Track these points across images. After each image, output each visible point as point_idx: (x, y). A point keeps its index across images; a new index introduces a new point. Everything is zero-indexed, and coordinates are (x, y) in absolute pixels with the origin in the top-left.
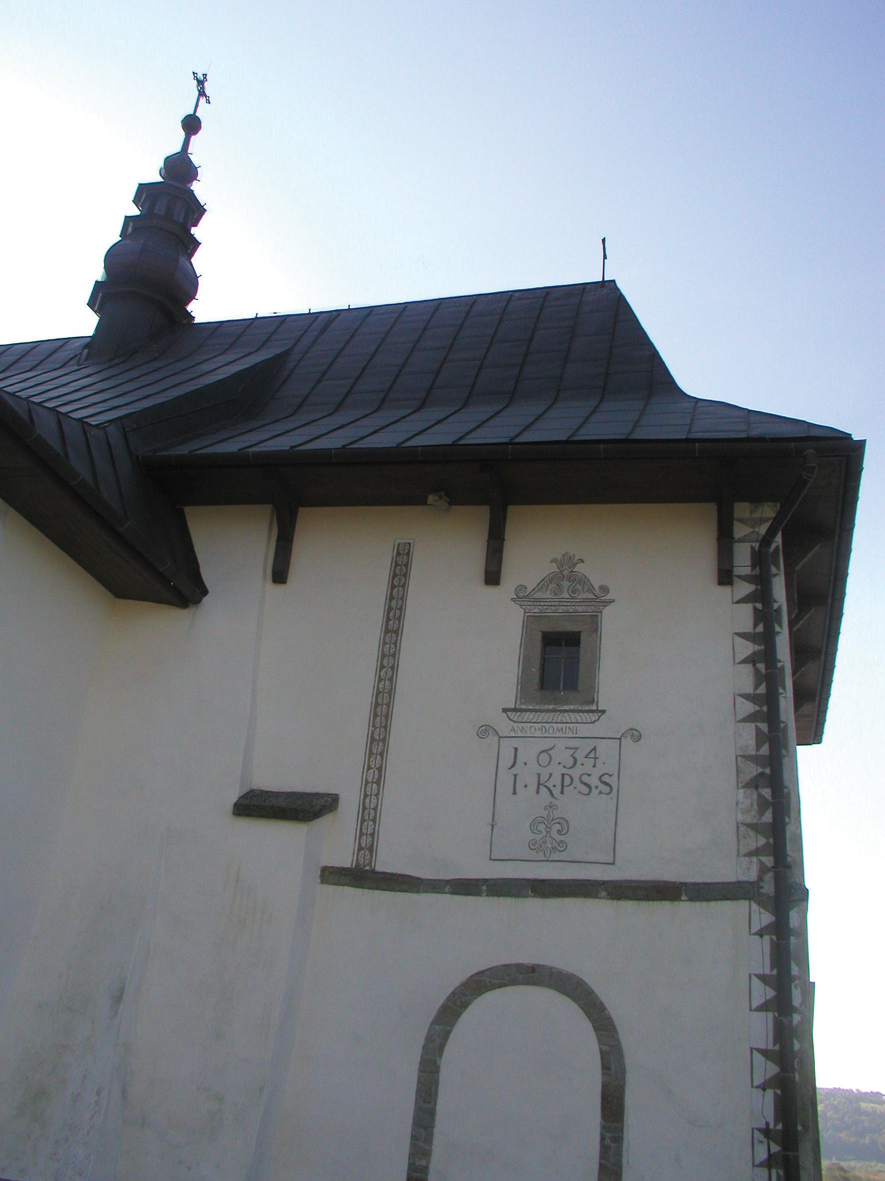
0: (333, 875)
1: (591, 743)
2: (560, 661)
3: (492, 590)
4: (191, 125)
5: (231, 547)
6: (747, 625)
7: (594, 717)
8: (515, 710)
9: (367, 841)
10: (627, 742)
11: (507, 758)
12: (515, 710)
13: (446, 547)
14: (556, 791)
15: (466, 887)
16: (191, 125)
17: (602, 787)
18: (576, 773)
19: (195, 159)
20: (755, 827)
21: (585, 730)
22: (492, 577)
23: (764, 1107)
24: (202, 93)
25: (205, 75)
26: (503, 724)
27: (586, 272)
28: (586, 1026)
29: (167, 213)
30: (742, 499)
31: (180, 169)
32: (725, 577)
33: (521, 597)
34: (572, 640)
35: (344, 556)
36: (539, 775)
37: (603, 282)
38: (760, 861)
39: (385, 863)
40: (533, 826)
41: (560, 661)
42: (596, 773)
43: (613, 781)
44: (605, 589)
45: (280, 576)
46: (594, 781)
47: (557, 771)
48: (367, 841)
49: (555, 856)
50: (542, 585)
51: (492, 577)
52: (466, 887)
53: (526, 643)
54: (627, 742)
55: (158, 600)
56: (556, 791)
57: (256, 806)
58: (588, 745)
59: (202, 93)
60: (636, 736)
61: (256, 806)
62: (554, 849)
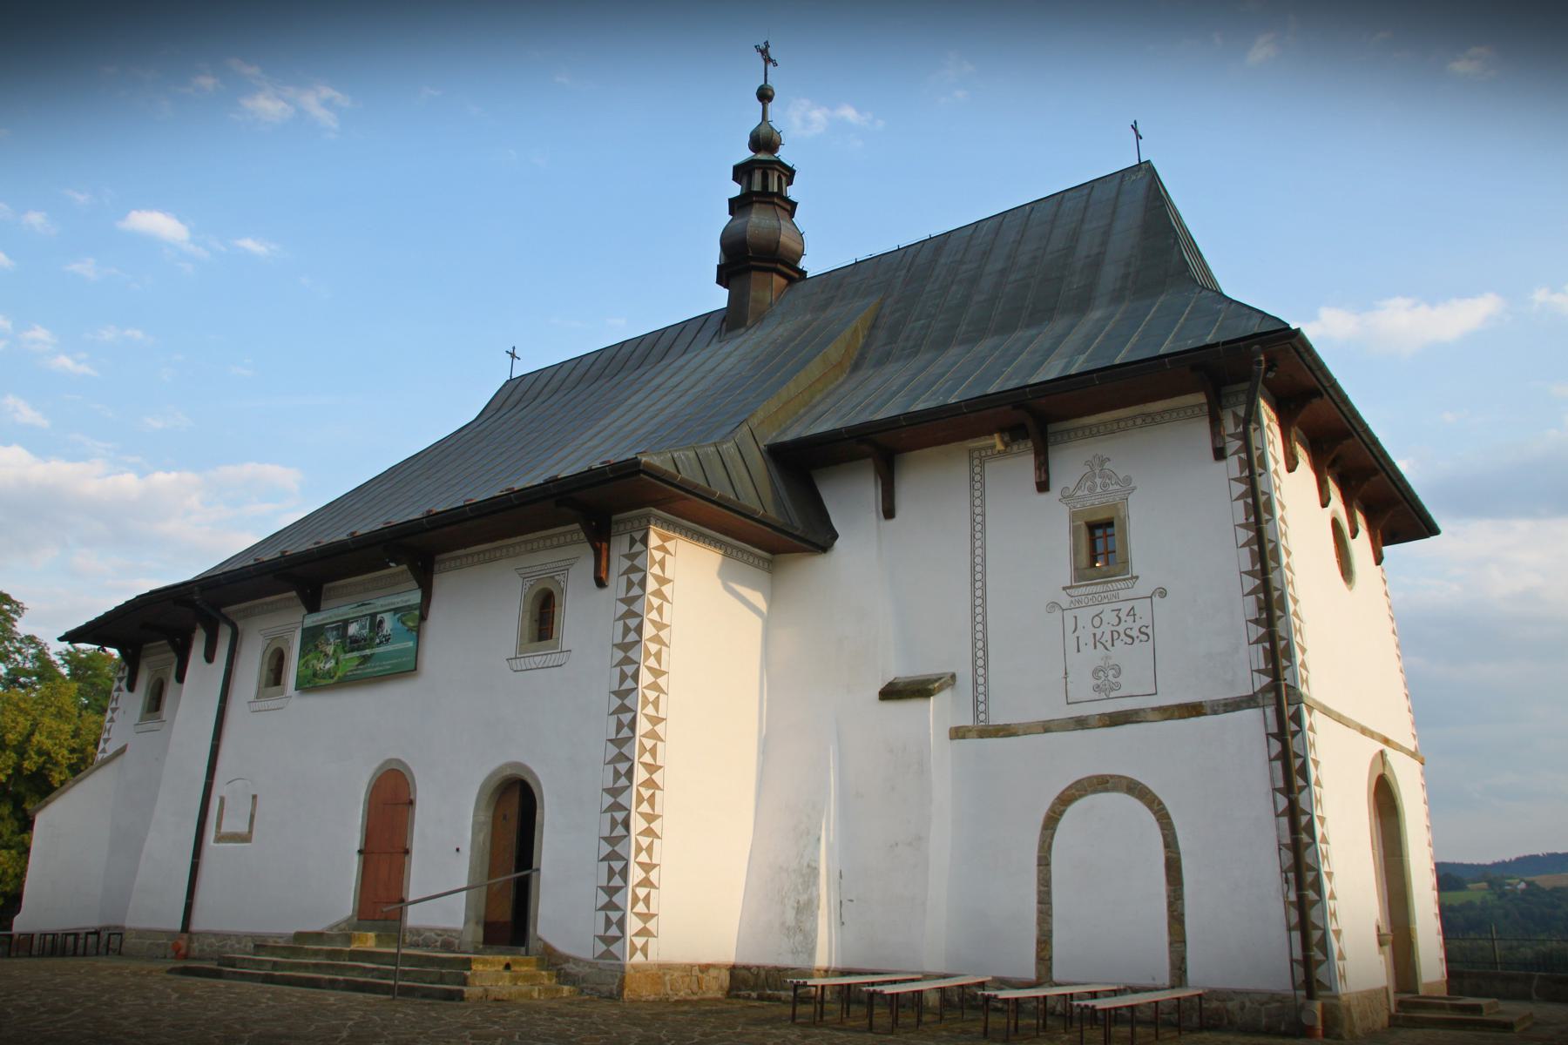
0: (958, 733)
1: (1130, 604)
2: (1100, 542)
3: (1044, 496)
4: (765, 95)
7: (1129, 583)
8: (1071, 587)
9: (979, 701)
10: (1156, 599)
11: (1070, 625)
12: (1071, 587)
14: (1109, 645)
15: (1047, 727)
16: (765, 95)
17: (1144, 637)
18: (1121, 629)
19: (776, 126)
21: (1123, 594)
22: (1043, 486)
24: (768, 60)
25: (766, 43)
26: (1065, 601)
28: (1072, 811)
30: (1208, 397)
31: (764, 141)
32: (1219, 454)
33: (1065, 497)
34: (1109, 524)
35: (935, 493)
36: (1387, 508)
39: (998, 718)
40: (1095, 672)
41: (1100, 542)
42: (1136, 627)
43: (1149, 631)
44: (1128, 480)
45: (889, 512)
46: (1134, 633)
47: (1107, 629)
48: (979, 701)
49: (1113, 694)
50: (1078, 487)
51: (1043, 486)
52: (1047, 727)
53: (1075, 532)
54: (1156, 599)
55: (804, 551)
56: (1109, 645)
58: (1125, 607)
59: (768, 60)
60: (1163, 593)
61: (891, 693)
62: (1112, 689)
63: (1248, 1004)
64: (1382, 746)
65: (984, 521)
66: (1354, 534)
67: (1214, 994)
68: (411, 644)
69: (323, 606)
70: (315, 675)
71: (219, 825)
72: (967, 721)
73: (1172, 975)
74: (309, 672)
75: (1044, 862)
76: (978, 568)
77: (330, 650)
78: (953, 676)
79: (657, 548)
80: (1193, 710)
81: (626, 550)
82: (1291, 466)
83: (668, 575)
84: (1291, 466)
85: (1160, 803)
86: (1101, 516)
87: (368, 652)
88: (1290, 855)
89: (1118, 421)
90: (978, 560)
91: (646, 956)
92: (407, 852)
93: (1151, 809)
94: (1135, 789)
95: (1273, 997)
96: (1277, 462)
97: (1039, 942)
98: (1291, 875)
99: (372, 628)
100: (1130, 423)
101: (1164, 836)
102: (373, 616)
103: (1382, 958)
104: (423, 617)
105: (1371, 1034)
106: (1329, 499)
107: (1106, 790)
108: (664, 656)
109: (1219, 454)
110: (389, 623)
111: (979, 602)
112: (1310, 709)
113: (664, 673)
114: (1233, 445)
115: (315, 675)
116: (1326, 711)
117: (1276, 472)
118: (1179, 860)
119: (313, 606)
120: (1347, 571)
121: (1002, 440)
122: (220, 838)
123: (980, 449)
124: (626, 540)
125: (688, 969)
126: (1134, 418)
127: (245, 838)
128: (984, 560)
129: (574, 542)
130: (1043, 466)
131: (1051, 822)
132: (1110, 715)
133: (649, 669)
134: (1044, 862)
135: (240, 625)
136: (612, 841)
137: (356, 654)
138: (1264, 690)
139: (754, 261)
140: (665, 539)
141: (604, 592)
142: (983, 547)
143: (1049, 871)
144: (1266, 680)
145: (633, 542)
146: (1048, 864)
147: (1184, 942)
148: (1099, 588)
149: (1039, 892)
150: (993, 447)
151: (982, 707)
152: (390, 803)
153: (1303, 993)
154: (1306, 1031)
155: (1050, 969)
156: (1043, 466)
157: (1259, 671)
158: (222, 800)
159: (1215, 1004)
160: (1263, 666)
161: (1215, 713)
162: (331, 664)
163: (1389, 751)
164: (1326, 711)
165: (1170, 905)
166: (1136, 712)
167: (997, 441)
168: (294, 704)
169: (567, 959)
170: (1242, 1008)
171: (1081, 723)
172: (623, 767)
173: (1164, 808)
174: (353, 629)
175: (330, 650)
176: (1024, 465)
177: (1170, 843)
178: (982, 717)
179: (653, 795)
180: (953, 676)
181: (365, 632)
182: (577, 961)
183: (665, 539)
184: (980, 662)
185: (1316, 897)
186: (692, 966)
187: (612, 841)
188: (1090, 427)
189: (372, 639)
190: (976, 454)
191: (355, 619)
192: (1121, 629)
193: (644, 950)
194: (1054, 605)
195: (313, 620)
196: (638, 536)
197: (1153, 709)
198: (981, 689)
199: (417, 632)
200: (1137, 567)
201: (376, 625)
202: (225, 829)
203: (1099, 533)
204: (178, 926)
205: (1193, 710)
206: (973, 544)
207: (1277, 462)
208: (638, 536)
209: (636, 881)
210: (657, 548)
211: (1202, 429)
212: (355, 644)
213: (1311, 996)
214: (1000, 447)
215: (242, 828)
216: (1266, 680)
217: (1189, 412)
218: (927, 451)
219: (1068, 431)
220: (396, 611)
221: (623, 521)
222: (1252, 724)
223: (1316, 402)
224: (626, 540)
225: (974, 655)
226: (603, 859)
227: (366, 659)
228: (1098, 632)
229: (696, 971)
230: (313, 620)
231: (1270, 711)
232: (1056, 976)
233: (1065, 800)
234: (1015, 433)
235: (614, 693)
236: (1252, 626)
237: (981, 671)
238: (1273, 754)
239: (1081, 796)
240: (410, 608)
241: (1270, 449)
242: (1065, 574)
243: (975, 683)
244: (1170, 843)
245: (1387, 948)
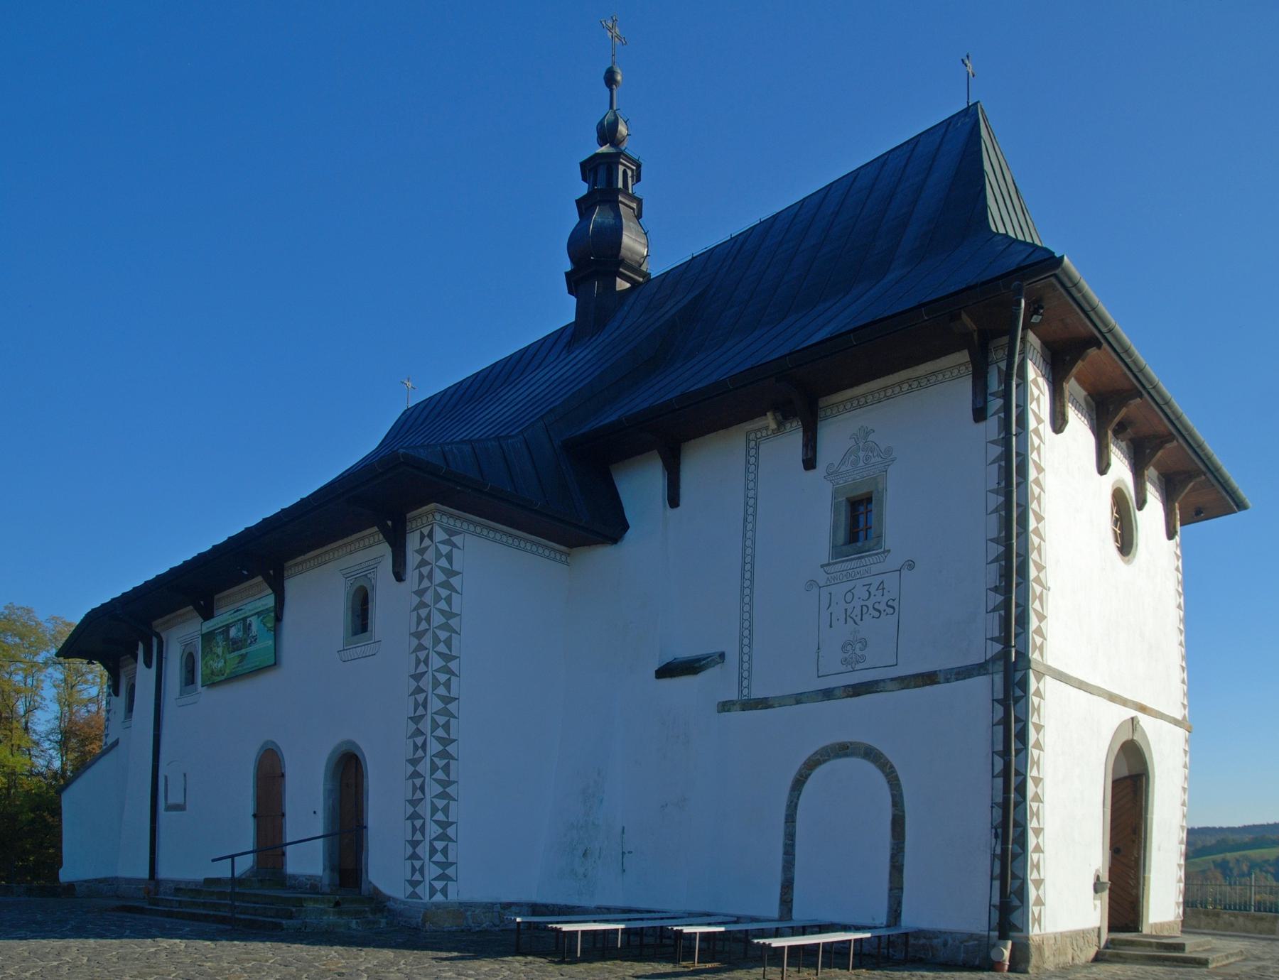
2: (858, 520)
3: (811, 473)
4: (610, 79)
5: (639, 486)
8: (829, 564)
12: (829, 564)
14: (858, 619)
15: (798, 699)
22: (810, 464)
26: (822, 578)
31: (607, 133)
32: (980, 414)
39: (757, 693)
41: (858, 520)
42: (885, 599)
43: (895, 604)
46: (882, 607)
49: (858, 667)
50: (842, 462)
51: (810, 464)
52: (798, 699)
55: (603, 543)
56: (858, 619)
58: (875, 582)
60: (911, 565)
61: (668, 671)
62: (858, 662)
63: (950, 942)
64: (1133, 713)
65: (755, 503)
66: (1141, 503)
67: (919, 933)
68: (271, 643)
69: (216, 613)
70: (212, 673)
72: (734, 696)
73: (781, 911)
74: (209, 671)
75: (790, 819)
76: (749, 551)
77: (219, 651)
78: (722, 655)
79: (443, 542)
80: (929, 679)
81: (417, 546)
82: (1059, 423)
83: (456, 567)
84: (1059, 423)
85: (892, 767)
86: (863, 490)
87: (243, 651)
88: (1000, 811)
89: (884, 389)
90: (749, 543)
91: (446, 896)
92: (283, 815)
93: (883, 772)
94: (871, 754)
95: (971, 936)
96: (1039, 421)
97: (783, 887)
98: (999, 831)
99: (245, 632)
100: (897, 389)
101: (893, 796)
102: (244, 619)
103: (1098, 903)
104: (278, 619)
105: (1065, 971)
106: (1108, 465)
107: (846, 755)
108: (455, 642)
110: (255, 623)
111: (747, 583)
112: (1040, 676)
113: (455, 658)
115: (212, 673)
116: (1062, 677)
117: (1037, 431)
118: (903, 817)
119: (207, 614)
120: (1125, 543)
121: (775, 418)
122: (170, 808)
123: (755, 431)
125: (489, 907)
126: (900, 384)
128: (754, 543)
129: (376, 544)
131: (799, 783)
132: (853, 686)
133: (439, 654)
134: (790, 819)
135: (163, 635)
136: (414, 803)
137: (236, 654)
138: (994, 660)
139: (594, 260)
140: (451, 533)
141: (402, 585)
142: (754, 531)
143: (794, 827)
144: (998, 647)
146: (794, 821)
147: (902, 889)
148: (854, 564)
149: (786, 845)
150: (767, 428)
151: (745, 683)
152: (270, 777)
153: (996, 933)
154: (994, 966)
155: (790, 910)
157: (992, 639)
159: (922, 941)
160: (996, 634)
161: (947, 681)
162: (221, 664)
163: (1144, 720)
164: (1062, 677)
165: (893, 856)
166: (876, 682)
168: (205, 696)
169: (389, 898)
170: (945, 944)
171: (828, 694)
172: (419, 741)
173: (894, 771)
176: (794, 439)
177: (897, 802)
178: (745, 692)
179: (448, 764)
180: (722, 655)
181: (240, 634)
182: (395, 900)
183: (451, 533)
184: (746, 641)
185: (1020, 851)
186: (493, 904)
187: (414, 803)
188: (857, 398)
189: (246, 640)
190: (752, 436)
192: (870, 603)
193: (444, 891)
194: (812, 583)
196: (426, 531)
197: (892, 680)
198: (746, 666)
199: (276, 631)
200: (888, 542)
201: (247, 628)
202: (171, 801)
204: (145, 874)
205: (929, 679)
206: (745, 527)
207: (1039, 421)
209: (433, 836)
210: (443, 542)
212: (235, 645)
213: (1004, 936)
214: (773, 426)
215: (180, 800)
216: (998, 647)
217: (948, 375)
218: (707, 437)
219: (837, 404)
220: (258, 614)
221: (415, 518)
222: (981, 689)
223: (1093, 352)
225: (741, 634)
226: (452, 823)
227: (243, 657)
228: (849, 607)
229: (498, 908)
231: (999, 678)
232: (800, 915)
233: (811, 765)
235: (411, 676)
236: (991, 594)
237: (746, 649)
238: (996, 720)
239: (825, 761)
241: (1033, 406)
243: (741, 660)
244: (897, 802)
245: (1106, 894)
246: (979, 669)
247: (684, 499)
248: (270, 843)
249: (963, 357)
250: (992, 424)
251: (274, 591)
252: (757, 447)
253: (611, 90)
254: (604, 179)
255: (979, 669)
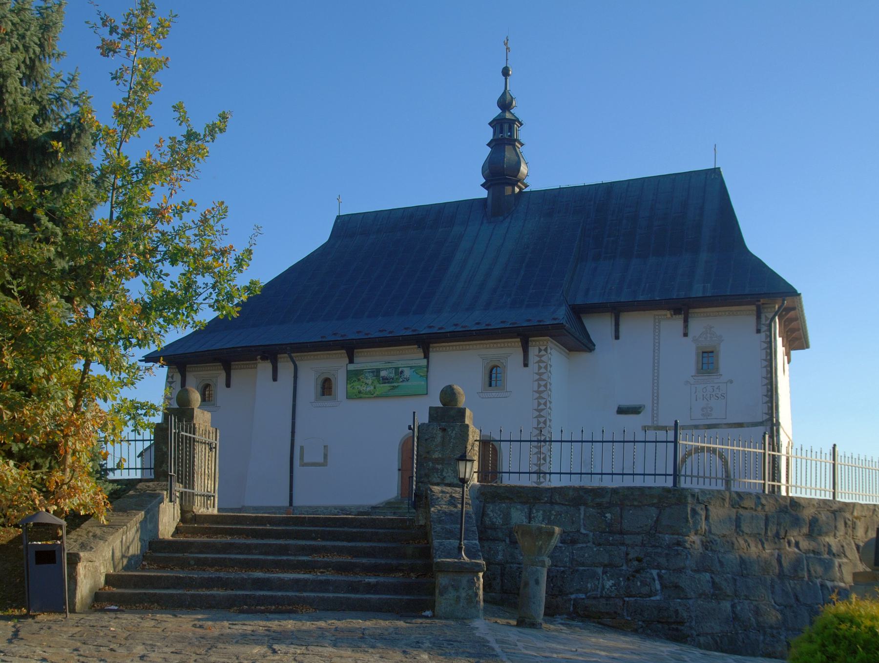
2: (707, 361)
4: (506, 72)
5: (598, 328)
6: (764, 375)
13: (672, 325)
16: (506, 72)
20: (766, 396)
22: (686, 335)
23: (764, 390)
27: (706, 164)
29: (504, 132)
31: (505, 104)
32: (758, 331)
35: (638, 328)
37: (715, 169)
38: (99, 600)
41: (707, 361)
54: (729, 384)
57: (621, 411)
60: (731, 382)
61: (621, 411)
71: (302, 458)
77: (369, 381)
80: (740, 425)
109: (758, 331)
114: (764, 328)
122: (303, 465)
124: (537, 349)
127: (324, 464)
130: (686, 326)
138: (766, 420)
139: (500, 172)
144: (768, 417)
145: (540, 350)
156: (686, 326)
158: (302, 448)
167: (668, 313)
171: (696, 427)
174: (383, 373)
175: (369, 381)
176: (679, 322)
191: (386, 369)
195: (351, 367)
196: (543, 348)
203: (705, 355)
205: (740, 425)
208: (543, 348)
211: (752, 320)
212: (385, 380)
214: (669, 316)
216: (768, 417)
220: (411, 367)
224: (536, 350)
230: (351, 367)
234: (677, 311)
240: (421, 367)
242: (693, 372)
243: (653, 409)
246: (761, 424)
247: (621, 334)
248: (764, 491)
249: (754, 308)
250: (763, 335)
251: (424, 352)
252: (659, 323)
253: (506, 79)
254: (504, 132)
255: (761, 424)
